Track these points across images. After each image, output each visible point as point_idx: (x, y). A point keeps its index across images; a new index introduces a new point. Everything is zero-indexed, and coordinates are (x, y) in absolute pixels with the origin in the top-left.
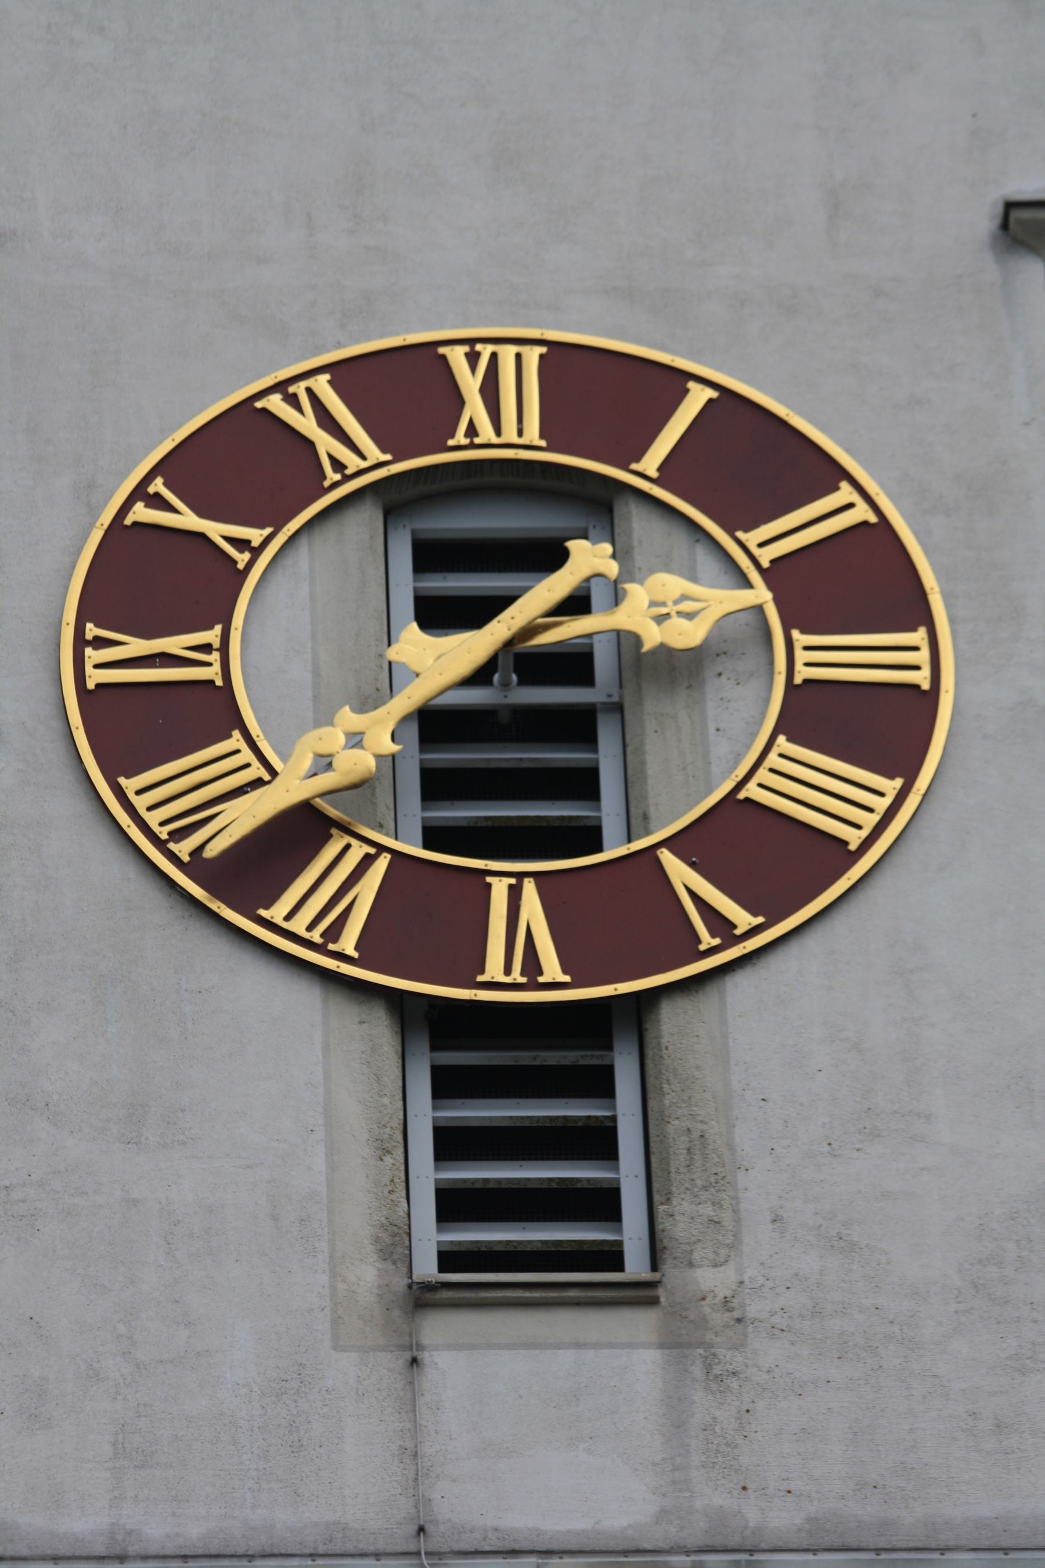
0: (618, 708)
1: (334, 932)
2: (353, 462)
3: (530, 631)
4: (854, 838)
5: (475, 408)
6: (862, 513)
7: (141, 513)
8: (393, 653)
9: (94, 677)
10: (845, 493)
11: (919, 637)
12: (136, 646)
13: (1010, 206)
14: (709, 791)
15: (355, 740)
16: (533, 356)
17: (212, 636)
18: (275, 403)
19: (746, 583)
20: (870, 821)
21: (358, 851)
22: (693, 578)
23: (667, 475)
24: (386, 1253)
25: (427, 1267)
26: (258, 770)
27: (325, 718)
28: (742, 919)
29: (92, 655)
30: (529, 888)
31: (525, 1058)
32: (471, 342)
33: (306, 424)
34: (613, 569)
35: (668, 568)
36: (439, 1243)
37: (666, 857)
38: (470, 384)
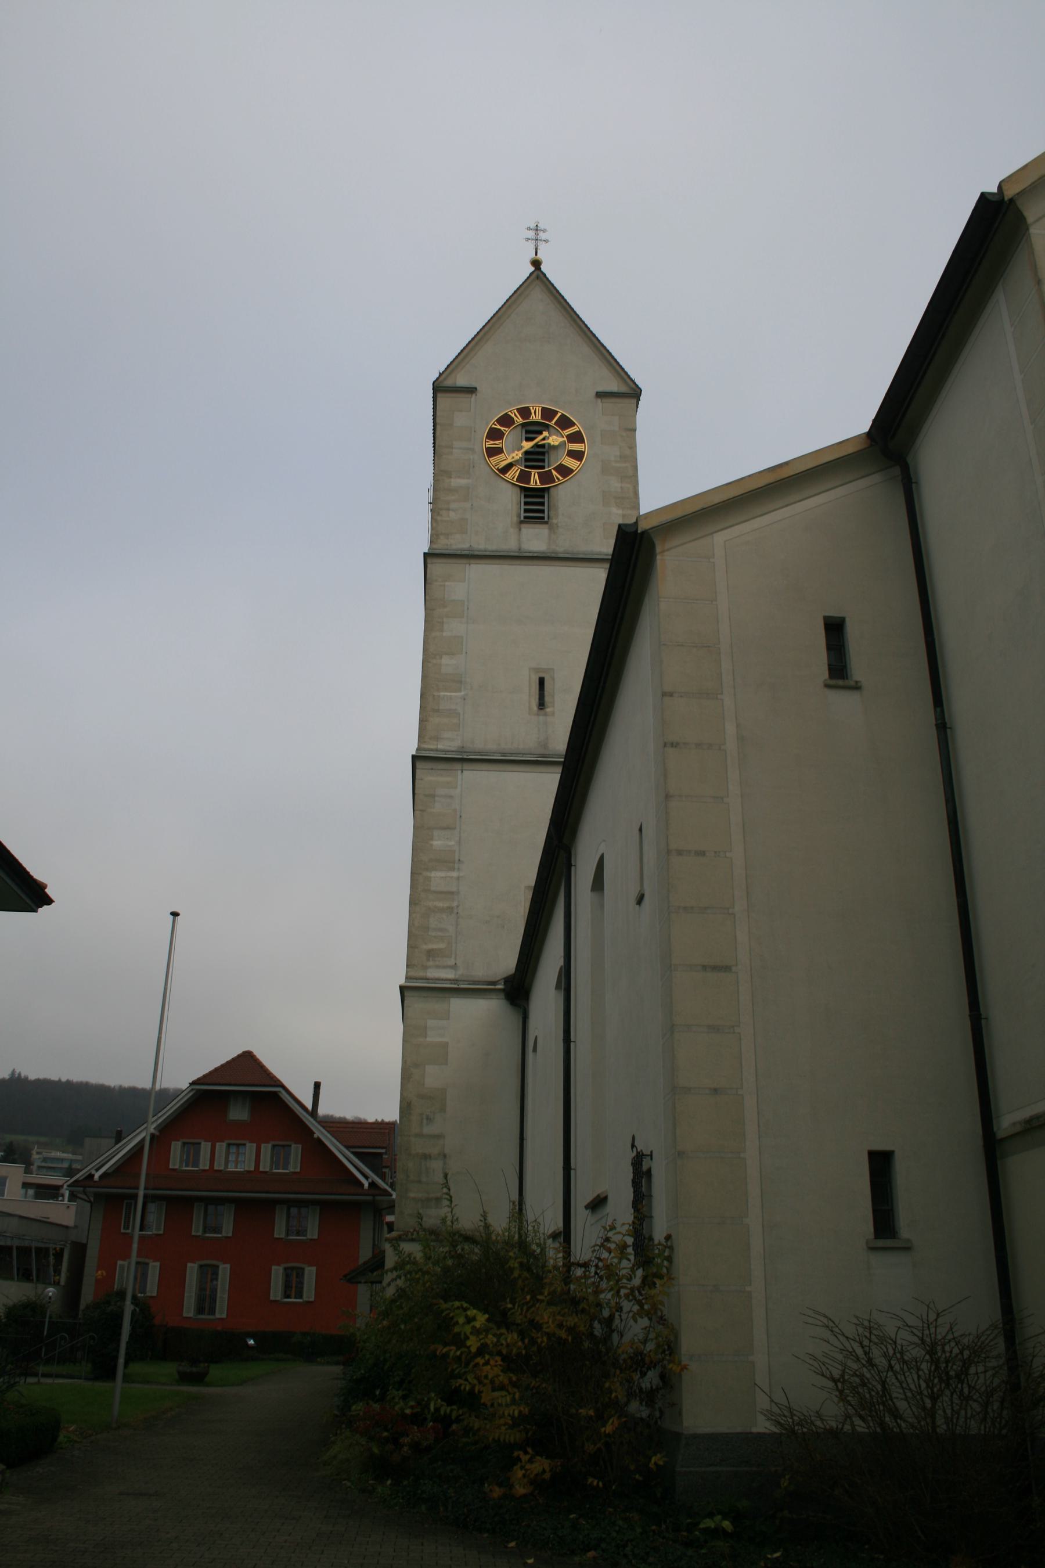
0: (548, 452)
1: (513, 478)
2: (518, 421)
3: (539, 442)
4: (574, 469)
5: (533, 414)
6: (577, 429)
7: (493, 426)
8: (522, 444)
9: (487, 446)
10: (576, 427)
11: (583, 445)
12: (492, 442)
13: (597, 393)
14: (556, 463)
15: (517, 455)
16: (540, 408)
17: (501, 441)
18: (510, 413)
19: (563, 437)
20: (576, 467)
21: (517, 468)
22: (557, 436)
23: (555, 424)
24: (517, 516)
25: (522, 518)
26: (505, 458)
27: (513, 452)
28: (561, 478)
29: (487, 443)
30: (536, 473)
31: (131, 1223)
32: (533, 406)
33: (513, 416)
34: (548, 435)
35: (555, 435)
36: (140, 1235)
37: (552, 470)
38: (533, 411)
